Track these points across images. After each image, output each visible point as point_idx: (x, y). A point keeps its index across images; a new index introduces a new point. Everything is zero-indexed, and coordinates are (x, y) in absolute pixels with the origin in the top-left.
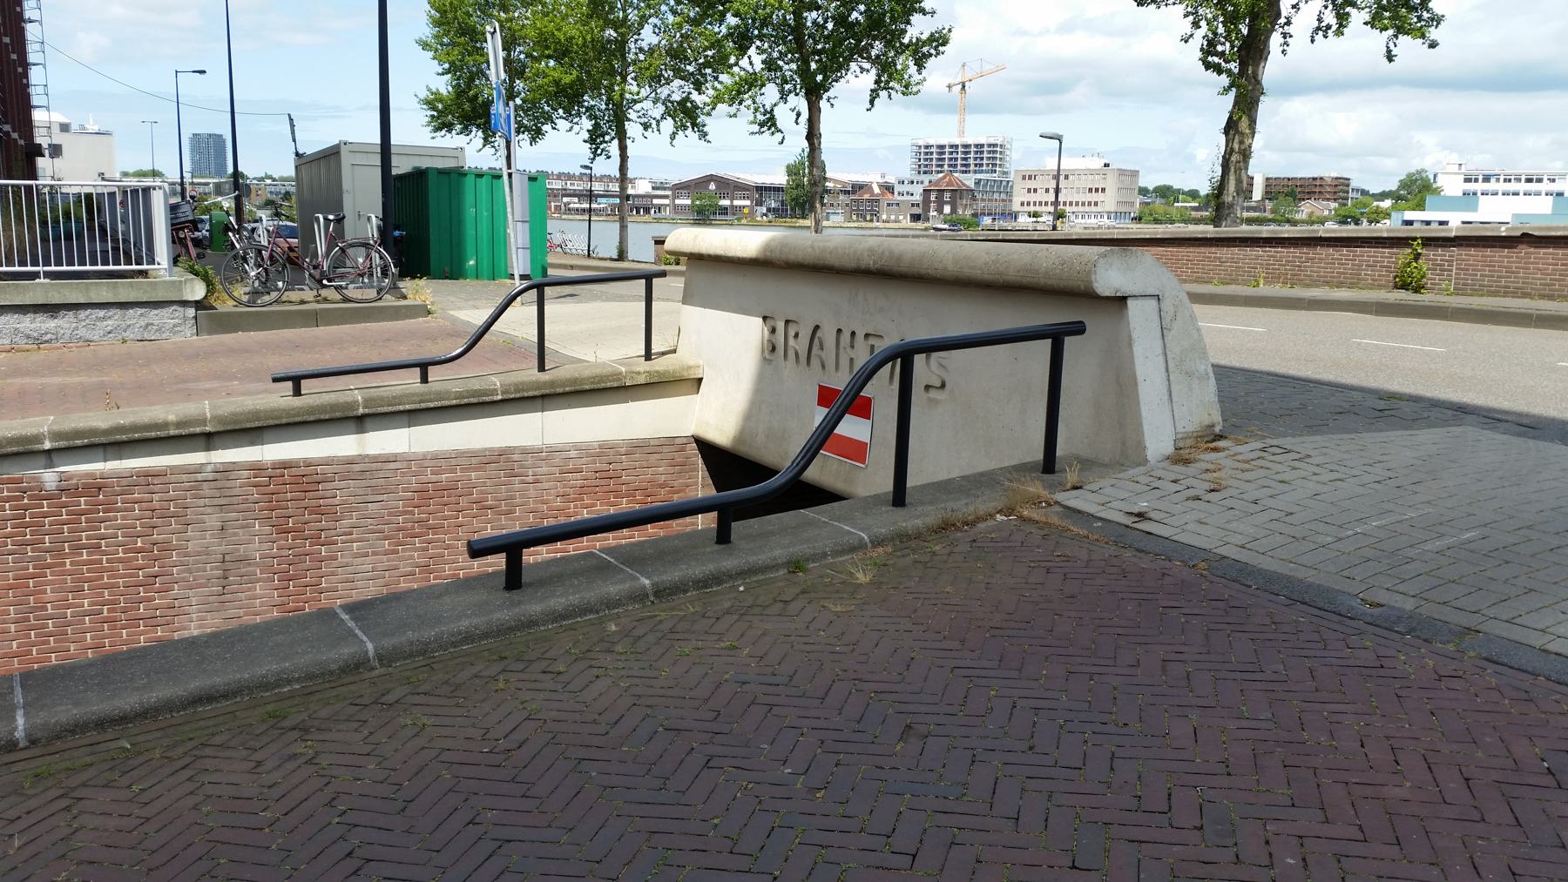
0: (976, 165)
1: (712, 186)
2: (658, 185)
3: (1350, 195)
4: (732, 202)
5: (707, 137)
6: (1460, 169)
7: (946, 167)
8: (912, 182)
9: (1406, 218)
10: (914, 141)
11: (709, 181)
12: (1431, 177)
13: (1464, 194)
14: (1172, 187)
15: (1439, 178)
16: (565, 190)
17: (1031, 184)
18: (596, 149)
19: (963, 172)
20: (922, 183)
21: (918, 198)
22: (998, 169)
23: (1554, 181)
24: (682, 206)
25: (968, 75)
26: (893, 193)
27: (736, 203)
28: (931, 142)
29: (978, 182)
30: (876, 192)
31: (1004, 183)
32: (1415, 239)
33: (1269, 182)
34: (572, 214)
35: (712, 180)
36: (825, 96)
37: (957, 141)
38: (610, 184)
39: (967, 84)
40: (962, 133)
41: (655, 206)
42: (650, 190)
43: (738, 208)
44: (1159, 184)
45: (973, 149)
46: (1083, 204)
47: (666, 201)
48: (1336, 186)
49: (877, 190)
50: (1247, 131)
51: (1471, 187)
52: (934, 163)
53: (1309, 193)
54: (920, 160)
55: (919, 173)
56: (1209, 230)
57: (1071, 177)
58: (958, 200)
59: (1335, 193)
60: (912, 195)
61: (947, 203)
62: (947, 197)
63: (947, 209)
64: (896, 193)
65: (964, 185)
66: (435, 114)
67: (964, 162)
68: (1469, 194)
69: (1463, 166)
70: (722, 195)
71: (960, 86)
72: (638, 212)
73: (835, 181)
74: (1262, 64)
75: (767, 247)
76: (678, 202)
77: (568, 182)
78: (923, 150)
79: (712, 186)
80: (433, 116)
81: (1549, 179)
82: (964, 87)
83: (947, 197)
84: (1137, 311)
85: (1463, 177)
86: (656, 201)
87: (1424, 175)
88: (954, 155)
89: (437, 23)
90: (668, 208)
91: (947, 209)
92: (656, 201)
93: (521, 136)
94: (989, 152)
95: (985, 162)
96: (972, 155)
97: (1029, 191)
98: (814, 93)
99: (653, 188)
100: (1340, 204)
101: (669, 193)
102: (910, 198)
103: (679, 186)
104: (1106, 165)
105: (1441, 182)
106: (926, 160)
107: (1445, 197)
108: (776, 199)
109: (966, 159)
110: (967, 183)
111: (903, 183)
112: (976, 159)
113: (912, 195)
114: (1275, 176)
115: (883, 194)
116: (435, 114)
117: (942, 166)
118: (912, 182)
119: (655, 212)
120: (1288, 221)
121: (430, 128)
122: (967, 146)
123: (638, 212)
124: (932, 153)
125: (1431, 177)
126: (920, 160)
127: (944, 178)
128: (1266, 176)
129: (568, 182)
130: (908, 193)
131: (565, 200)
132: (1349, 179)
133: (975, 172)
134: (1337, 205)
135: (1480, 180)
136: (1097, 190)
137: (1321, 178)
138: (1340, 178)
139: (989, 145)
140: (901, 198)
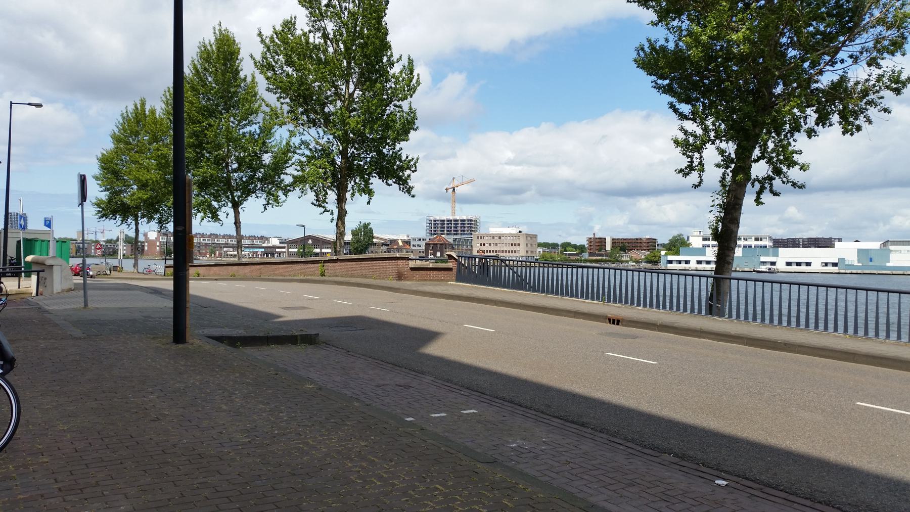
0: (461, 231)
1: (310, 242)
2: (283, 241)
3: (657, 248)
4: (321, 250)
5: (330, 213)
6: (700, 234)
7: (445, 232)
8: (420, 240)
9: (668, 259)
10: (428, 218)
11: (308, 239)
12: (686, 239)
13: (703, 247)
14: (570, 243)
15: (690, 238)
16: (227, 244)
17: (482, 241)
18: (161, 227)
19: (448, 234)
20: (425, 240)
21: (423, 248)
22: (473, 233)
23: (746, 240)
24: (293, 252)
25: (456, 183)
26: (410, 245)
27: (323, 251)
28: (438, 218)
29: (455, 240)
30: (400, 245)
31: (470, 241)
32: (321, 261)
33: (614, 241)
34: (228, 258)
35: (310, 238)
36: (240, 207)
37: (451, 218)
38: (255, 241)
39: (456, 189)
40: (454, 214)
41: (277, 253)
42: (278, 243)
43: (291, 254)
44: (564, 242)
45: (459, 222)
46: (509, 252)
47: (284, 250)
48: (648, 243)
49: (401, 244)
50: (341, 226)
51: (707, 243)
52: (439, 229)
53: (635, 246)
54: (431, 227)
55: (431, 234)
56: (335, 257)
57: (502, 238)
58: (444, 249)
59: (648, 246)
60: (420, 246)
61: (438, 251)
62: (438, 247)
63: (438, 254)
64: (411, 245)
65: (447, 241)
66: (101, 209)
67: (455, 229)
68: (746, 247)
69: (702, 232)
70: (316, 246)
71: (452, 189)
72: (267, 256)
73: (378, 238)
74: (344, 204)
75: (32, 259)
76: (290, 250)
77: (229, 240)
78: (433, 222)
79: (310, 242)
80: (99, 211)
81: (744, 239)
82: (454, 190)
83: (438, 247)
84: (56, 269)
85: (702, 238)
86: (277, 250)
87: (681, 237)
88: (450, 225)
89: (103, 168)
90: (284, 254)
91: (438, 254)
92: (277, 250)
93: (143, 220)
94: (468, 224)
95: (466, 229)
96: (459, 225)
97: (481, 245)
98: (236, 206)
99: (280, 243)
100: (651, 252)
101: (286, 245)
102: (419, 248)
103: (291, 242)
104: (520, 232)
105: (691, 240)
106: (435, 228)
107: (693, 248)
108: (346, 248)
109: (456, 227)
110: (449, 240)
111: (415, 240)
112: (461, 227)
113: (420, 246)
114: (617, 238)
115: (404, 246)
116: (101, 209)
117: (443, 231)
118: (420, 240)
119: (277, 256)
120: (618, 261)
121: (97, 217)
122: (463, 221)
123: (267, 256)
124: (438, 224)
125: (686, 239)
126: (431, 227)
127: (436, 237)
128: (612, 238)
129: (229, 240)
130: (418, 246)
131: (225, 249)
132: (655, 239)
133: (461, 234)
134: (649, 253)
135: (711, 239)
136: (515, 245)
137: (640, 239)
138: (651, 239)
139: (468, 220)
140: (414, 248)
